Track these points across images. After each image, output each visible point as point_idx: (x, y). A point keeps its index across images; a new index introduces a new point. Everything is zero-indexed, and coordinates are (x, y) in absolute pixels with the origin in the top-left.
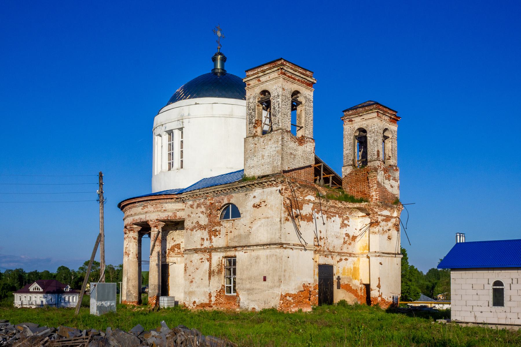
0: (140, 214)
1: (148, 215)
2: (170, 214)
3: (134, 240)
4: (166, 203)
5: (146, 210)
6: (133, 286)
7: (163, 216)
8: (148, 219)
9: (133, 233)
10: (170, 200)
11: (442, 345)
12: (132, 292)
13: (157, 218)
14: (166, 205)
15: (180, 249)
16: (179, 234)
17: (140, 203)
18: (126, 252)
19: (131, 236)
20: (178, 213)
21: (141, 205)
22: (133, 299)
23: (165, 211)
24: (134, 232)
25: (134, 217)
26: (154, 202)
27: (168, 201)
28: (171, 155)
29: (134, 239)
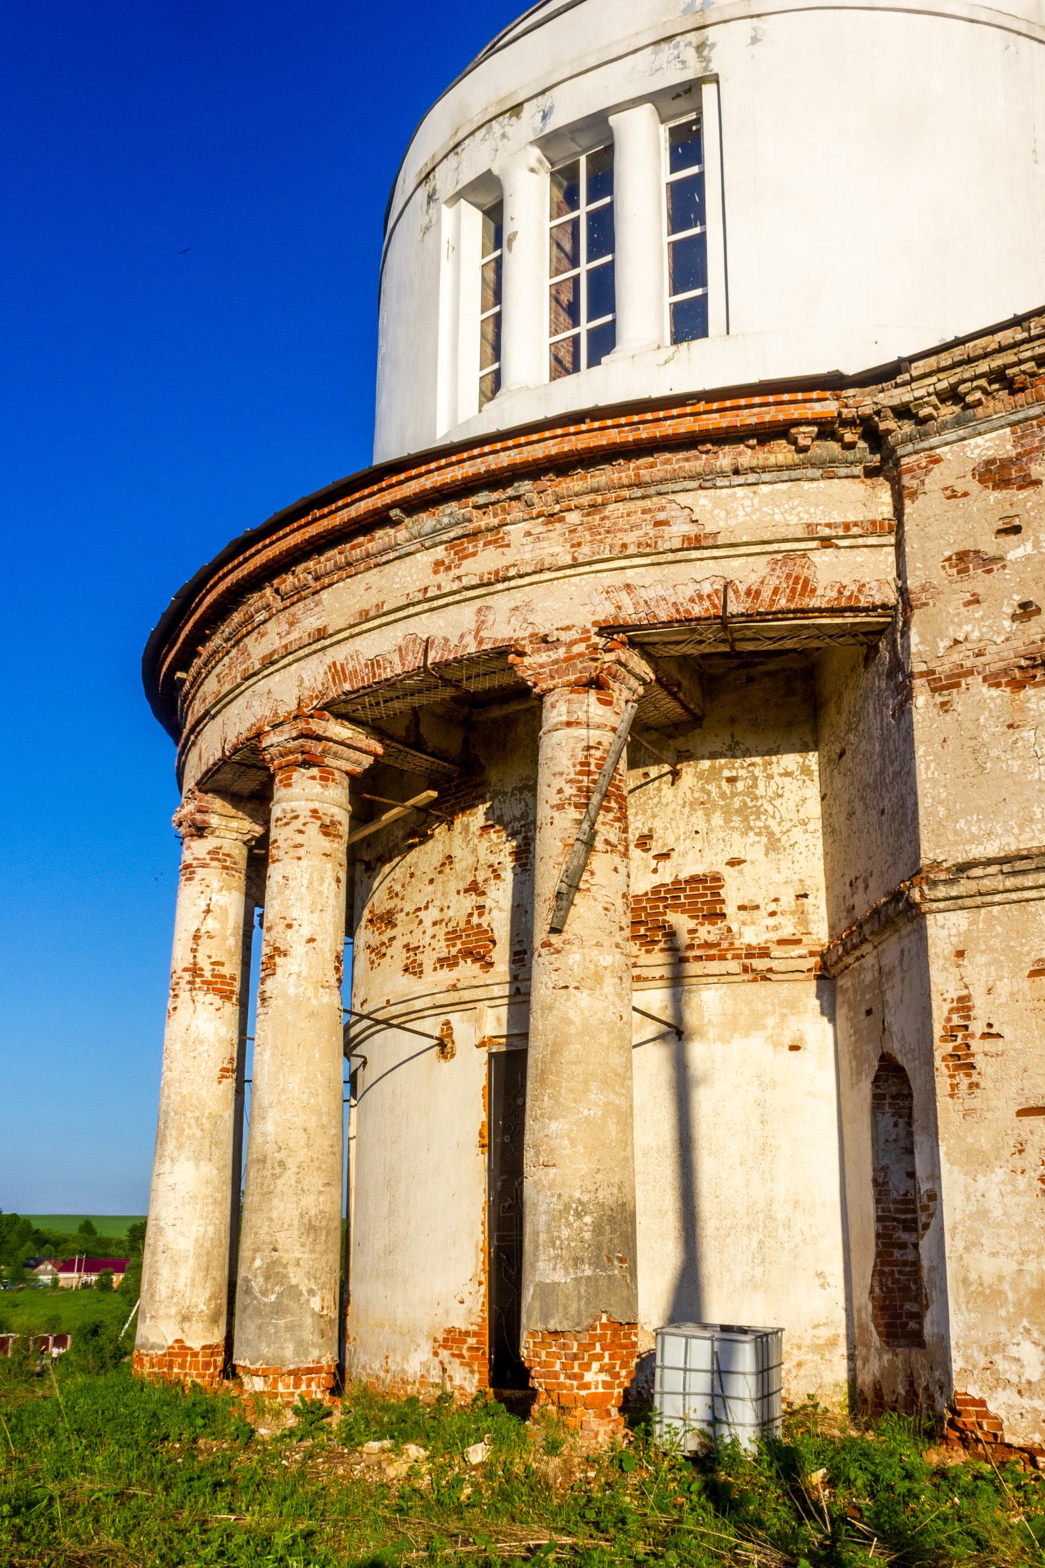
0: (430, 601)
1: (502, 602)
2: (749, 572)
3: (325, 843)
4: (705, 480)
5: (485, 560)
6: (311, 1228)
7: (673, 592)
8: (503, 627)
9: (316, 787)
10: (747, 455)
11: (822, 1560)
12: (296, 1277)
13: (605, 612)
14: (702, 501)
15: (716, 916)
16: (704, 804)
17: (426, 521)
18: (195, 970)
19: (304, 808)
20: (822, 558)
21: (426, 541)
22: (301, 1346)
23: (695, 543)
24: (326, 778)
25: (339, 654)
26: (575, 483)
27: (725, 458)
28: (494, 345)
29: (326, 830)
